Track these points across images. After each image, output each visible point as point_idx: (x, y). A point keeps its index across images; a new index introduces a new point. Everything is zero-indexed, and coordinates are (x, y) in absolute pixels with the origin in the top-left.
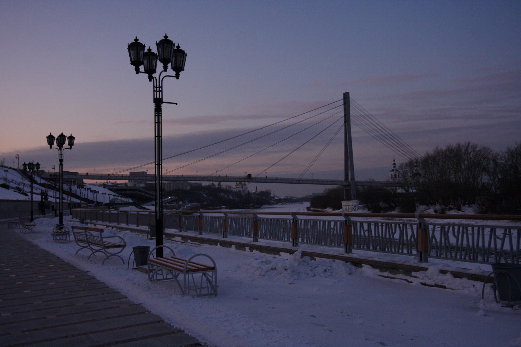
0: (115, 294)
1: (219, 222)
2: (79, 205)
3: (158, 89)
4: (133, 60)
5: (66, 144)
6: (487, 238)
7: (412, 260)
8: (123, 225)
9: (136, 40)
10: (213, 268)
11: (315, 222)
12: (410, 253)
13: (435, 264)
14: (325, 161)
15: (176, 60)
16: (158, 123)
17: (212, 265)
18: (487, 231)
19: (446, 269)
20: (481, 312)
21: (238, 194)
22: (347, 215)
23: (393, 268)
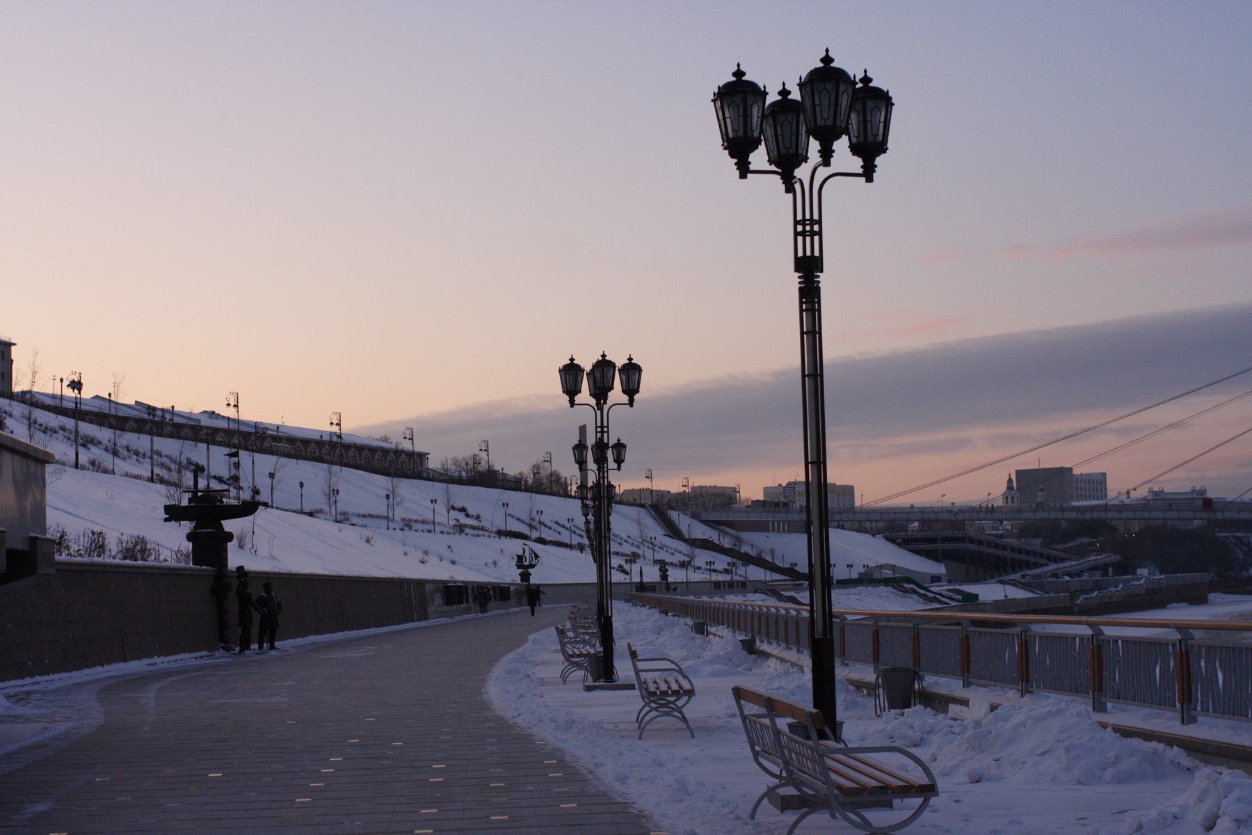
4: (731, 135)
5: (617, 394)
15: (864, 122)
16: (812, 334)
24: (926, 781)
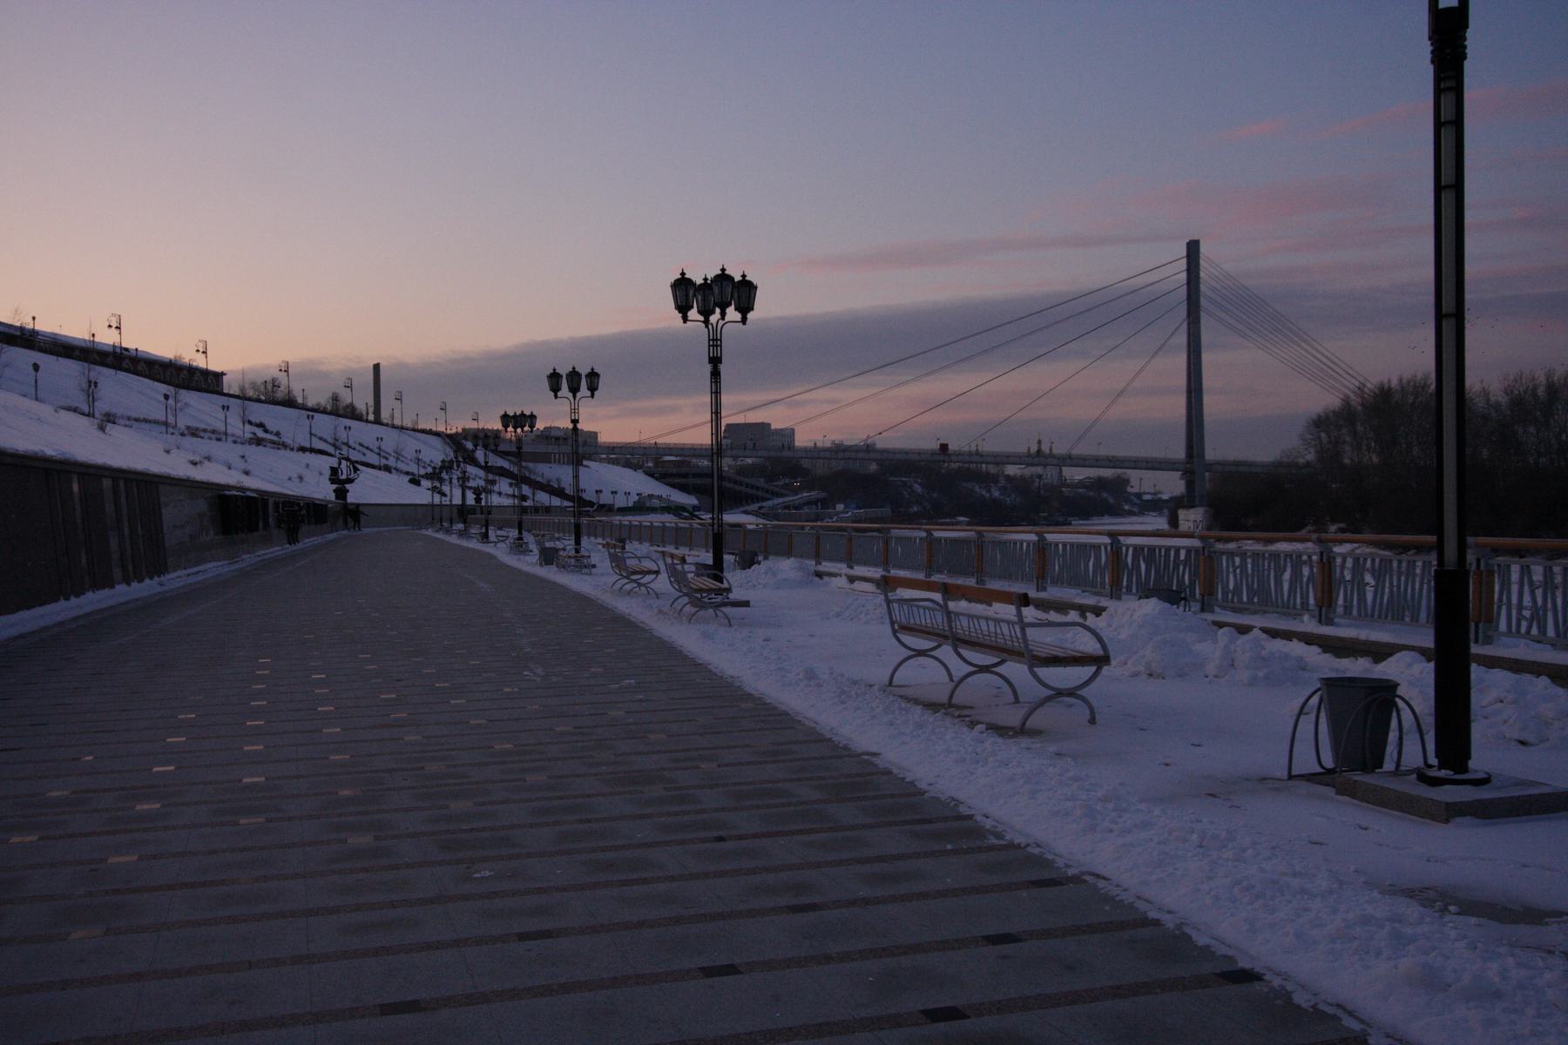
1: (1098, 559)
24: (1101, 653)
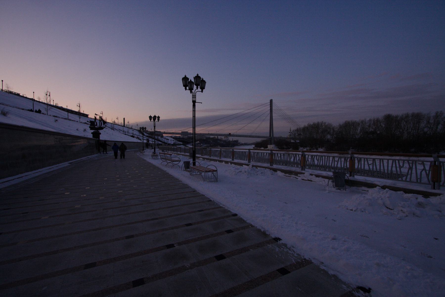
0: (177, 180)
2: (161, 145)
3: (194, 96)
6: (331, 162)
7: (299, 170)
8: (179, 153)
9: (185, 76)
10: (216, 171)
11: (258, 153)
12: (297, 167)
13: (308, 172)
14: (262, 128)
16: (194, 111)
17: (216, 169)
18: (331, 158)
19: (313, 173)
20: (327, 191)
21: (225, 141)
22: (271, 150)
23: (290, 172)
